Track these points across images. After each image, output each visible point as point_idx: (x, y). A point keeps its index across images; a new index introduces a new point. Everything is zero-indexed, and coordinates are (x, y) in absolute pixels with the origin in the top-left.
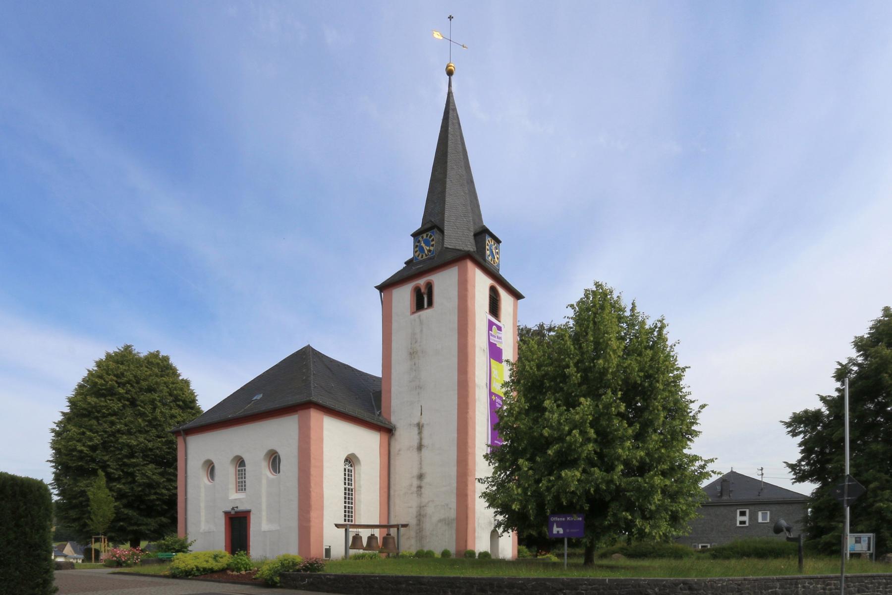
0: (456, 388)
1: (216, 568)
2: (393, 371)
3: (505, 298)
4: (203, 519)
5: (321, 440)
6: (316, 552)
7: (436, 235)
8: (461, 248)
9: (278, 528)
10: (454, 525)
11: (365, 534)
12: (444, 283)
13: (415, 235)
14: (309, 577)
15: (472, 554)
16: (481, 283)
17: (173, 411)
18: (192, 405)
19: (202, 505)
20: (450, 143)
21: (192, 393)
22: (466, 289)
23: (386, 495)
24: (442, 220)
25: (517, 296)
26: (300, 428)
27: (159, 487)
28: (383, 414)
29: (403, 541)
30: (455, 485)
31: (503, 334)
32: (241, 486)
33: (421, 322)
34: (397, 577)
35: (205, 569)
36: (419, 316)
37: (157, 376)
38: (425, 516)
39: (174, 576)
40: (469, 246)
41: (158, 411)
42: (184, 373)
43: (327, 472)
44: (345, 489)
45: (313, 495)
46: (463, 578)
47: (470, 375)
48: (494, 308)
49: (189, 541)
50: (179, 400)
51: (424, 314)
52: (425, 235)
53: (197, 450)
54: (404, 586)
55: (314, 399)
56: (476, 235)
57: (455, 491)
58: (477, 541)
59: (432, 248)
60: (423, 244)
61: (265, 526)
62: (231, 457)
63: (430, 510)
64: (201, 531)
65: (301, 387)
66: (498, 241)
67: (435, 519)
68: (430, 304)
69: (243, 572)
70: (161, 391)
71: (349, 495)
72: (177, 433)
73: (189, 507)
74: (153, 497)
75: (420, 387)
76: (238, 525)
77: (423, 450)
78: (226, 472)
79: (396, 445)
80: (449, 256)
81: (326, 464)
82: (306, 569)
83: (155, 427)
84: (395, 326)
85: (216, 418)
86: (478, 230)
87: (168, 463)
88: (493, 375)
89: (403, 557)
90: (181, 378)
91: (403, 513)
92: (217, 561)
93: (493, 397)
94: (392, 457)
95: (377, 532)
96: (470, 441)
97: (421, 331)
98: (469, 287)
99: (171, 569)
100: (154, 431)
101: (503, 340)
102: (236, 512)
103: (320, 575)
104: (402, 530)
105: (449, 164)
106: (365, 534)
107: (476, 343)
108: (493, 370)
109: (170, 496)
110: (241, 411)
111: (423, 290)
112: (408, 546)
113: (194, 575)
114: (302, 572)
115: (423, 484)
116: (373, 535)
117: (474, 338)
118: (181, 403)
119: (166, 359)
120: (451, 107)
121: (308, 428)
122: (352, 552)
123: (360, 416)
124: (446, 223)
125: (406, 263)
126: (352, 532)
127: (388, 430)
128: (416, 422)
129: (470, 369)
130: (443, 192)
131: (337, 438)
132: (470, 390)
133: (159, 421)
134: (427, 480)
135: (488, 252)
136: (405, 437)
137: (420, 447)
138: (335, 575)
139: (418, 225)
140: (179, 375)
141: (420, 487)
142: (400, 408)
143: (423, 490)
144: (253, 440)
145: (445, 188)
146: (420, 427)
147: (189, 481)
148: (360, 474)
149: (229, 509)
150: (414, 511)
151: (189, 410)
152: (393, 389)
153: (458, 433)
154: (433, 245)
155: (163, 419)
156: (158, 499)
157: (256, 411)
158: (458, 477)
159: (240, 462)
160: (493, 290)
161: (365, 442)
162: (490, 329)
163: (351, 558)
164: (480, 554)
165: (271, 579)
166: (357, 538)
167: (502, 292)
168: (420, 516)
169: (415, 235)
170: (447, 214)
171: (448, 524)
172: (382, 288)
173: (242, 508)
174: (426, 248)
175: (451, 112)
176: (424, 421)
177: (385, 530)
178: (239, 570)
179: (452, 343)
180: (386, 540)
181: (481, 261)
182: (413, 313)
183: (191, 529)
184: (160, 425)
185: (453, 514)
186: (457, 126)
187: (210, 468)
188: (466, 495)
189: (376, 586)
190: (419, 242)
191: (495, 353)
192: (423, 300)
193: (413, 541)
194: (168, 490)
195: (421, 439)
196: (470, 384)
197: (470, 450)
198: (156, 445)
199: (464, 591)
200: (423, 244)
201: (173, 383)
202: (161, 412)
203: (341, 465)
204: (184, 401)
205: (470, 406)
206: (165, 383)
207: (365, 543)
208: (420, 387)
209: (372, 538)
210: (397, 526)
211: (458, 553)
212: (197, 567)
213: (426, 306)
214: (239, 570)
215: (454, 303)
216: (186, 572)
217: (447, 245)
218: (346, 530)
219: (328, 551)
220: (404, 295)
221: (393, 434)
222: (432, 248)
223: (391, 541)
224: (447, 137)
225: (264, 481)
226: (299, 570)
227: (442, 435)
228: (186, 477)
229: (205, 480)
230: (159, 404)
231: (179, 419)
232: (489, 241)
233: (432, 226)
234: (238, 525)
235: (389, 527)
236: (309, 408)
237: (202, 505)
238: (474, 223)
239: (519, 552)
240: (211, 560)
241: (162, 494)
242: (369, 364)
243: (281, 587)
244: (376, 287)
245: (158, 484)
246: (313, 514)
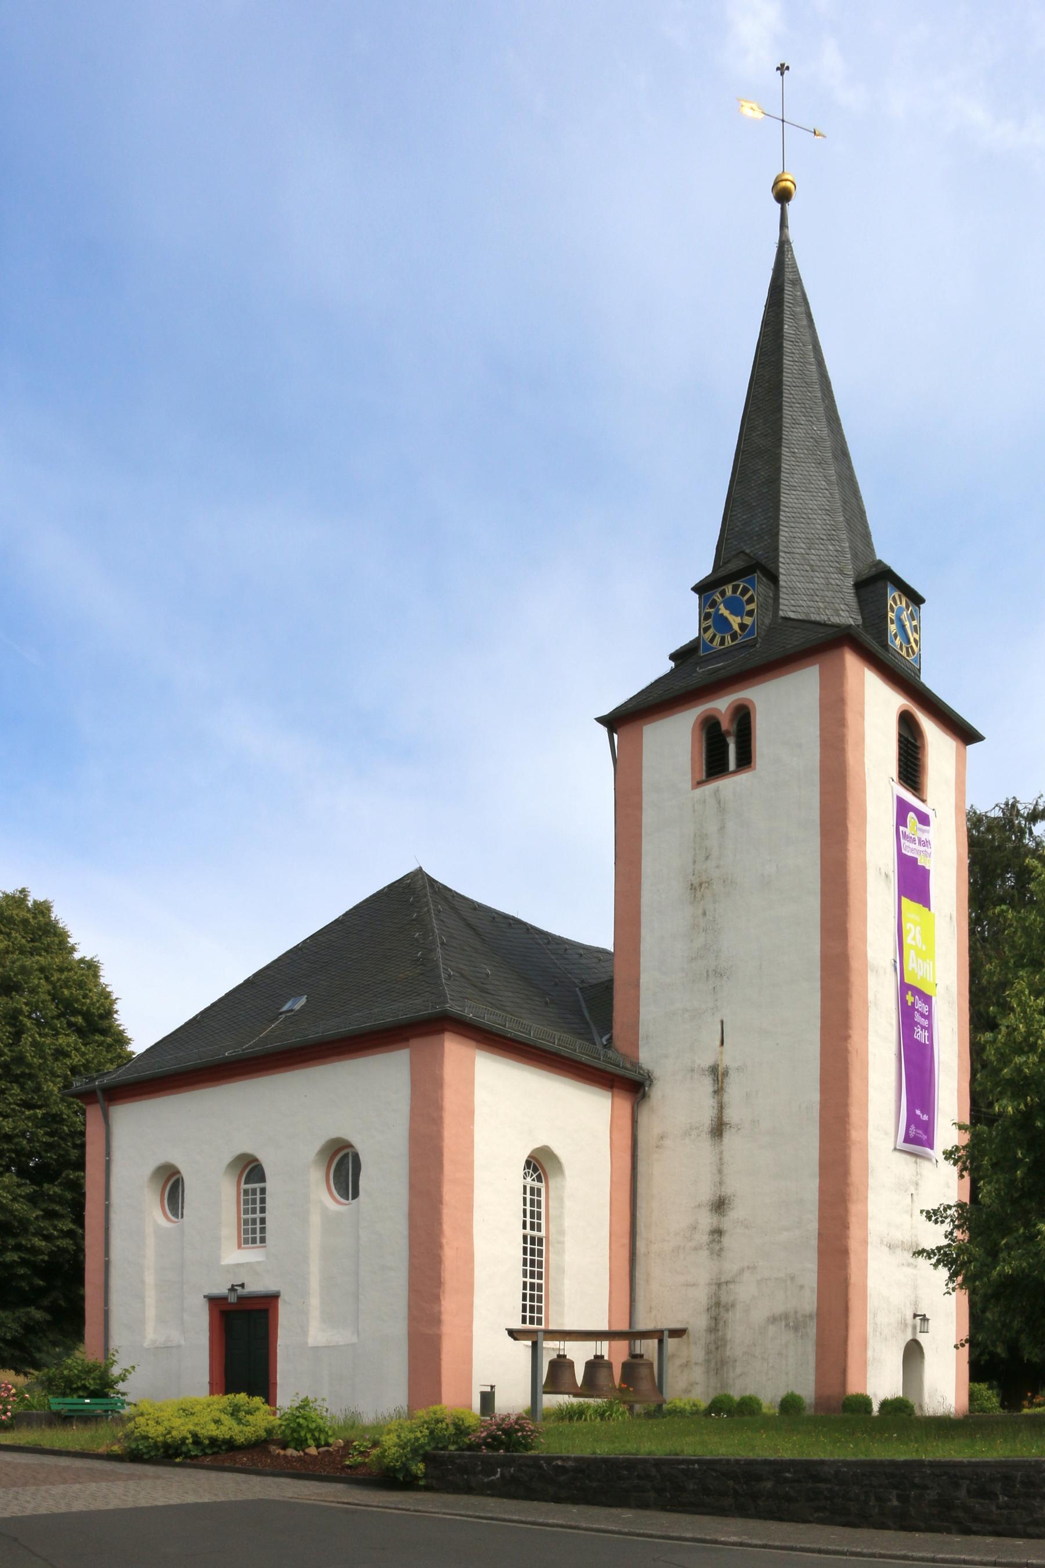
0: (818, 974)
1: (240, 1439)
2: (644, 932)
3: (936, 740)
4: (151, 1312)
5: (469, 1113)
6: (458, 1401)
7: (759, 589)
8: (823, 618)
9: (354, 1339)
10: (812, 1330)
11: (580, 1354)
12: (784, 707)
13: (700, 589)
14: (505, 1463)
15: (863, 1403)
16: (878, 705)
17: (62, 1040)
18: (105, 1024)
19: (150, 1278)
20: (787, 361)
21: (107, 995)
22: (841, 722)
23: (625, 1254)
24: (774, 550)
25: (965, 734)
26: (416, 1083)
27: (25, 1230)
28: (618, 1043)
29: (672, 1370)
30: (815, 1225)
31: (931, 833)
32: (253, 1231)
33: (721, 806)
34: (751, 1463)
35: (213, 1441)
36: (717, 791)
37: (22, 952)
38: (730, 1307)
39: (134, 1457)
40: (845, 613)
41: (26, 1039)
42: (85, 944)
43: (482, 1195)
44: (525, 1237)
45: (449, 1253)
46: (932, 1464)
47: (853, 940)
48: (911, 768)
49: (116, 1371)
50: (76, 1012)
51: (730, 785)
52: (729, 589)
53: (135, 1142)
54: (769, 1485)
55: (453, 1007)
56: (860, 586)
57: (814, 1242)
58: (871, 1372)
59: (748, 621)
60: (724, 611)
61: (317, 1335)
62: (228, 1158)
63: (744, 1291)
64: (146, 1344)
65: (406, 978)
66: (916, 599)
67: (759, 1314)
68: (745, 760)
69: (313, 1451)
70: (33, 991)
71: (534, 1252)
72: (88, 1097)
73: (116, 1282)
74: (11, 1257)
75: (718, 973)
76: (244, 1334)
77: (727, 1136)
78: (214, 1196)
79: (652, 1123)
80: (795, 641)
81: (478, 1174)
82: (494, 1442)
83: (16, 1079)
84: (649, 817)
85: (169, 1064)
86: (866, 573)
87: (61, 1174)
88: (907, 941)
89: (676, 1413)
90: (77, 956)
91: (673, 1298)
92: (240, 1421)
93: (910, 998)
94: (641, 1154)
95: (603, 1348)
96: (854, 1112)
97: (722, 828)
98: (850, 717)
99: (127, 1436)
100: (16, 1089)
101: (933, 849)
102: (241, 1299)
103: (536, 1458)
104: (671, 1343)
105: (786, 412)
106: (580, 1354)
107: (869, 858)
108: (907, 926)
109: (51, 1254)
110: (249, 1037)
111: (725, 725)
112: (687, 1384)
113: (187, 1455)
114: (485, 1451)
115: (726, 1224)
116: (599, 1357)
117: (863, 844)
118: (79, 1020)
119: (43, 909)
120: (788, 276)
121: (438, 1083)
122: (551, 1401)
123: (565, 1051)
124: (783, 558)
125: (673, 657)
126: (551, 1348)
127: (631, 1085)
128: (707, 1061)
129: (853, 925)
130: (773, 482)
131: (509, 1110)
132: (855, 978)
133: (30, 1066)
134: (737, 1213)
135: (893, 628)
136: (678, 1103)
137: (719, 1129)
138: (577, 1460)
139: (704, 568)
140: (73, 949)
141: (718, 1233)
142: (662, 1029)
143: (726, 1240)
144: (287, 1115)
145: (778, 470)
146: (718, 1075)
147: (115, 1218)
148: (561, 1200)
149: (221, 1289)
150: (702, 1295)
151: (98, 1037)
152: (646, 979)
153: (823, 1092)
154: (750, 613)
155: (36, 1061)
156: (24, 1262)
157: (294, 1040)
158: (822, 1202)
159: (251, 1171)
160: (906, 721)
161: (575, 1117)
162: (901, 820)
163: (546, 1417)
164: (885, 1404)
165: (405, 1468)
166: (561, 1365)
167: (929, 728)
168: (718, 1310)
169: (700, 589)
170: (784, 535)
171: (796, 1329)
172: (613, 722)
173: (256, 1286)
174: (735, 621)
175: (788, 288)
176: (729, 1059)
177: (622, 1345)
178: (301, 1444)
179: (806, 859)
180: (633, 1366)
181: (875, 647)
182: (700, 783)
183: (119, 1338)
184: (31, 1076)
185: (808, 1302)
186: (805, 322)
187: (171, 1186)
188: (845, 1252)
189: (691, 1486)
190: (714, 604)
191: (913, 882)
192: (725, 750)
193: (698, 1374)
194: (47, 1238)
195: (721, 1107)
196: (855, 964)
197: (855, 1135)
198: (22, 1125)
199: (932, 1495)
200: (724, 611)
201: (61, 970)
202: (35, 1043)
203: (515, 1178)
204: (87, 1015)
205: (855, 1022)
206: (42, 970)
207: (579, 1378)
208: (718, 973)
209: (595, 1365)
210: (658, 1335)
211: (822, 1402)
212: (195, 1435)
213: (732, 765)
214: (301, 1444)
215: (809, 756)
216: (166, 1446)
217: (788, 608)
218: (535, 1346)
219: (488, 1399)
220: (674, 739)
221: (644, 1096)
222: (748, 621)
223: (644, 1372)
224: (780, 347)
225: (315, 1219)
226: (470, 1447)
227: (779, 1092)
228: (107, 1208)
229: (156, 1215)
230: (28, 1023)
231: (76, 1059)
232: (894, 599)
233: (744, 561)
234: (244, 1334)
235: (632, 1335)
236: (441, 1031)
237: (150, 1278)
238: (855, 556)
239: (972, 1396)
240: (226, 1419)
241: (34, 1250)
242: (583, 918)
243: (427, 1488)
244: (601, 720)
245: (24, 1223)
246: (449, 1305)
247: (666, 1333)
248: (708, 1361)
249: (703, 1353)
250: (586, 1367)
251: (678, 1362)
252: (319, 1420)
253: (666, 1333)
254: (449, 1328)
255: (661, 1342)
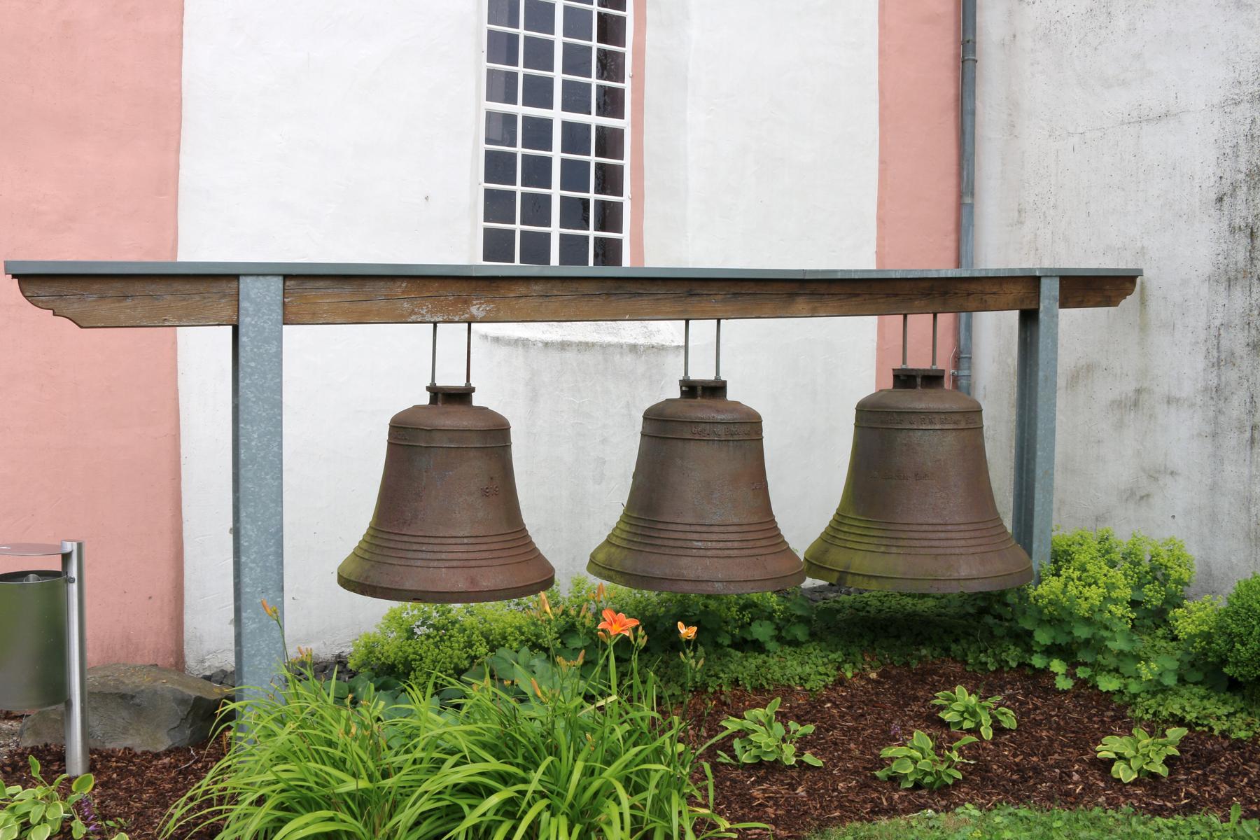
29: (1072, 422)
104: (1073, 328)
210: (1023, 293)
247: (1050, 290)
248: (1218, 393)
249: (1200, 363)
250: (859, 425)
251: (1106, 391)
252: (1217, 123)
253: (1050, 290)
254: (1041, 414)
255: (1029, 318)
